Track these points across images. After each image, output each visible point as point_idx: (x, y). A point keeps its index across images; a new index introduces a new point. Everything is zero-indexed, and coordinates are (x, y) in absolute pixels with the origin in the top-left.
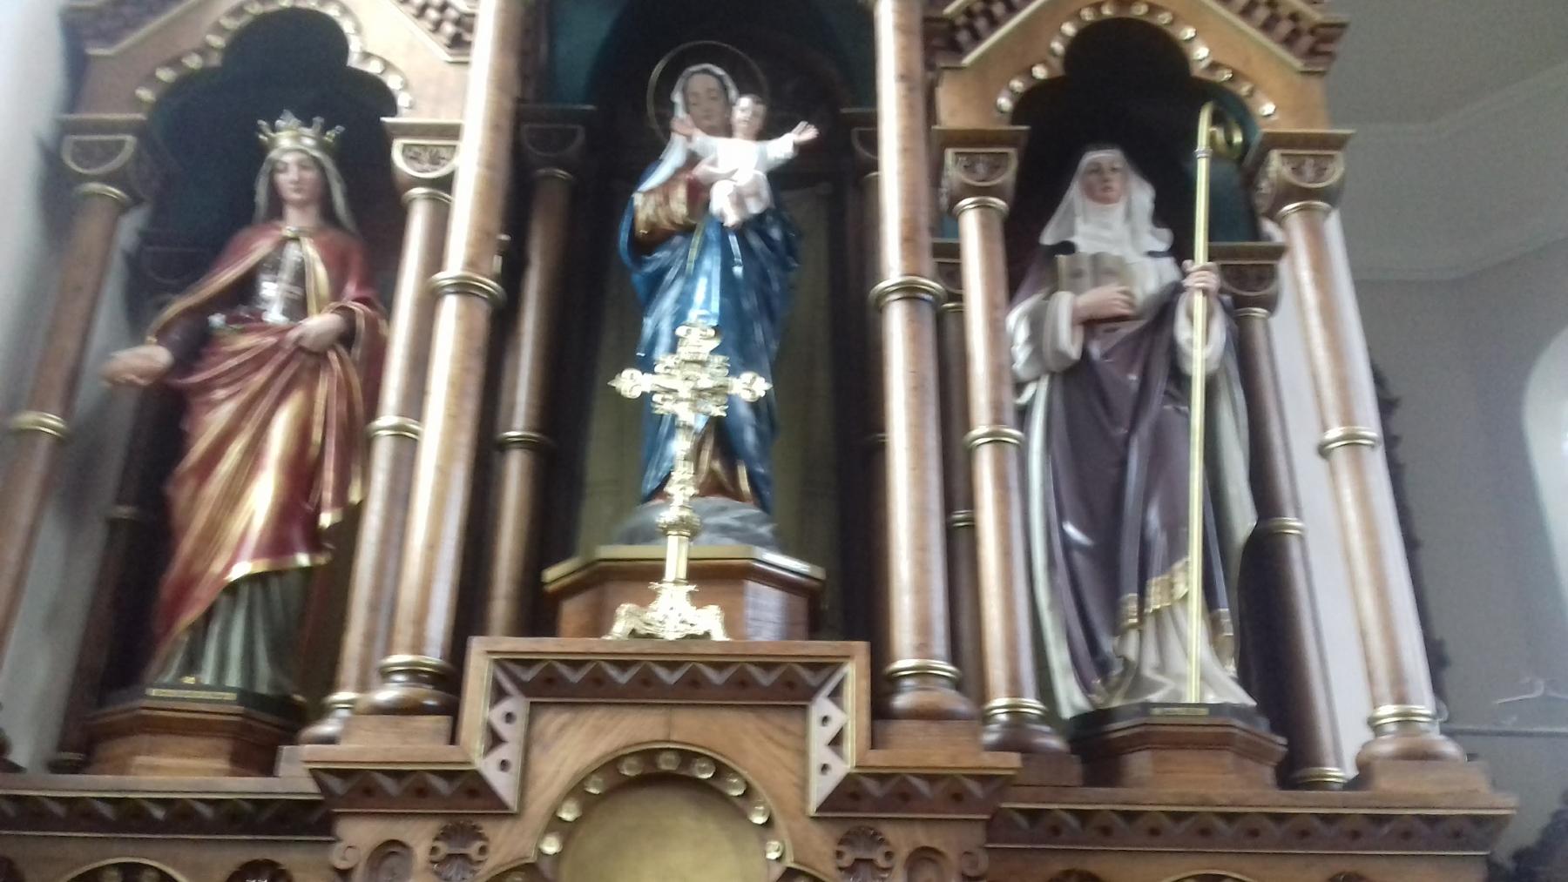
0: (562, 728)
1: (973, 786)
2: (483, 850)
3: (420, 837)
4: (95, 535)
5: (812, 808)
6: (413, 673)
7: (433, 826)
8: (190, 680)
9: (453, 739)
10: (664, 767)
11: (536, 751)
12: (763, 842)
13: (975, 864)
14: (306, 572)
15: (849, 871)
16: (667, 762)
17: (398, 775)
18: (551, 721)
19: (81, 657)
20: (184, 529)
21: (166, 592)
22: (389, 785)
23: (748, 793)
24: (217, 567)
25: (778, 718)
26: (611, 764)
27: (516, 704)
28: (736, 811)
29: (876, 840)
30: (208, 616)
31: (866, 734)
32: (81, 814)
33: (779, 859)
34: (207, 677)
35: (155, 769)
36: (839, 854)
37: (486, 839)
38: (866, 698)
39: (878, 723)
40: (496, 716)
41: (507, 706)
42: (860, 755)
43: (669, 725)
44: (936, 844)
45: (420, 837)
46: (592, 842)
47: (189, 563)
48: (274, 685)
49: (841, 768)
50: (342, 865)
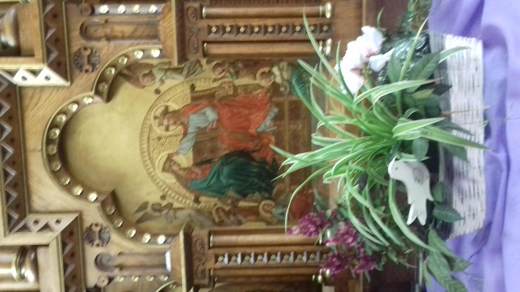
0: (40, 197)
1: (49, 8)
2: (97, 225)
3: (92, 252)
5: (68, 84)
6: (20, 265)
9: (47, 246)
10: (55, 151)
11: (52, 208)
12: (85, 106)
13: (86, 9)
15: (94, 66)
16: (53, 149)
17: (66, 266)
18: (37, 203)
22: (70, 269)
23: (63, 112)
25: (26, 101)
26: (56, 175)
27: (30, 219)
28: (73, 118)
29: (79, 54)
31: (28, 59)
33: (93, 98)
36: (87, 71)
37: (91, 225)
38: (10, 59)
39: (23, 52)
40: (35, 228)
41: (31, 224)
42: (38, 62)
43: (34, 151)
44: (79, 28)
45: (92, 252)
46: (93, 178)
49: (46, 71)
50: (106, 282)
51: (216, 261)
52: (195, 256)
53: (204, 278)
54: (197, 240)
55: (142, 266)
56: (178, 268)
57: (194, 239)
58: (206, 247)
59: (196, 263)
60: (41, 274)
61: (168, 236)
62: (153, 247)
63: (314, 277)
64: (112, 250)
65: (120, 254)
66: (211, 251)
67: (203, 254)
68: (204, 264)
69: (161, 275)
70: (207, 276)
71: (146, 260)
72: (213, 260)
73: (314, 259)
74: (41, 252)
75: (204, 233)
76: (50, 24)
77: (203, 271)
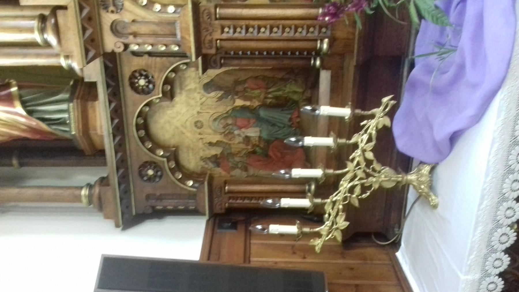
4: (26, 170)
6: (42, 30)
7: (103, 13)
8: (68, 122)
14: (20, 88)
17: (84, 30)
19: (73, 165)
20: (11, 136)
21: (38, 137)
24: (23, 120)
30: (43, 120)
32: (120, 147)
34: (66, 116)
35: (101, 127)
45: (108, 18)
47: (24, 131)
48: (67, 91)
50: (122, 48)
51: (223, 32)
52: (203, 26)
53: (211, 48)
54: (205, 10)
55: (155, 35)
56: (187, 37)
57: (202, 9)
58: (213, 17)
59: (204, 33)
60: (62, 36)
61: (177, 6)
62: (165, 16)
63: (312, 62)
64: (127, 17)
65: (134, 21)
66: (217, 22)
67: (210, 24)
68: (211, 35)
69: (172, 44)
70: (214, 45)
71: (157, 29)
72: (219, 31)
73: (312, 32)
74: (60, 13)
75: (212, 5)
76: (90, 47)
77: (211, 41)
